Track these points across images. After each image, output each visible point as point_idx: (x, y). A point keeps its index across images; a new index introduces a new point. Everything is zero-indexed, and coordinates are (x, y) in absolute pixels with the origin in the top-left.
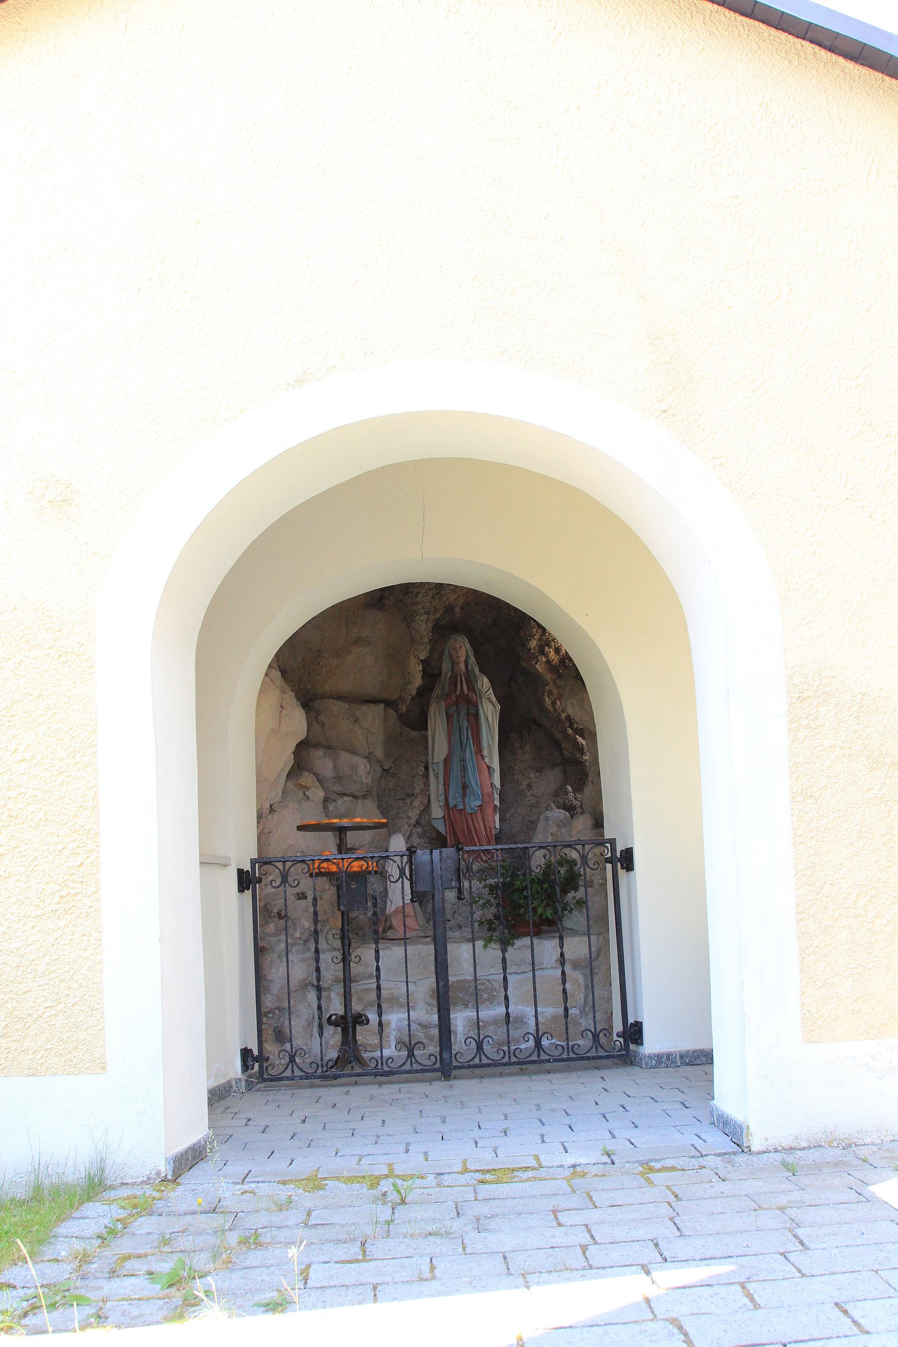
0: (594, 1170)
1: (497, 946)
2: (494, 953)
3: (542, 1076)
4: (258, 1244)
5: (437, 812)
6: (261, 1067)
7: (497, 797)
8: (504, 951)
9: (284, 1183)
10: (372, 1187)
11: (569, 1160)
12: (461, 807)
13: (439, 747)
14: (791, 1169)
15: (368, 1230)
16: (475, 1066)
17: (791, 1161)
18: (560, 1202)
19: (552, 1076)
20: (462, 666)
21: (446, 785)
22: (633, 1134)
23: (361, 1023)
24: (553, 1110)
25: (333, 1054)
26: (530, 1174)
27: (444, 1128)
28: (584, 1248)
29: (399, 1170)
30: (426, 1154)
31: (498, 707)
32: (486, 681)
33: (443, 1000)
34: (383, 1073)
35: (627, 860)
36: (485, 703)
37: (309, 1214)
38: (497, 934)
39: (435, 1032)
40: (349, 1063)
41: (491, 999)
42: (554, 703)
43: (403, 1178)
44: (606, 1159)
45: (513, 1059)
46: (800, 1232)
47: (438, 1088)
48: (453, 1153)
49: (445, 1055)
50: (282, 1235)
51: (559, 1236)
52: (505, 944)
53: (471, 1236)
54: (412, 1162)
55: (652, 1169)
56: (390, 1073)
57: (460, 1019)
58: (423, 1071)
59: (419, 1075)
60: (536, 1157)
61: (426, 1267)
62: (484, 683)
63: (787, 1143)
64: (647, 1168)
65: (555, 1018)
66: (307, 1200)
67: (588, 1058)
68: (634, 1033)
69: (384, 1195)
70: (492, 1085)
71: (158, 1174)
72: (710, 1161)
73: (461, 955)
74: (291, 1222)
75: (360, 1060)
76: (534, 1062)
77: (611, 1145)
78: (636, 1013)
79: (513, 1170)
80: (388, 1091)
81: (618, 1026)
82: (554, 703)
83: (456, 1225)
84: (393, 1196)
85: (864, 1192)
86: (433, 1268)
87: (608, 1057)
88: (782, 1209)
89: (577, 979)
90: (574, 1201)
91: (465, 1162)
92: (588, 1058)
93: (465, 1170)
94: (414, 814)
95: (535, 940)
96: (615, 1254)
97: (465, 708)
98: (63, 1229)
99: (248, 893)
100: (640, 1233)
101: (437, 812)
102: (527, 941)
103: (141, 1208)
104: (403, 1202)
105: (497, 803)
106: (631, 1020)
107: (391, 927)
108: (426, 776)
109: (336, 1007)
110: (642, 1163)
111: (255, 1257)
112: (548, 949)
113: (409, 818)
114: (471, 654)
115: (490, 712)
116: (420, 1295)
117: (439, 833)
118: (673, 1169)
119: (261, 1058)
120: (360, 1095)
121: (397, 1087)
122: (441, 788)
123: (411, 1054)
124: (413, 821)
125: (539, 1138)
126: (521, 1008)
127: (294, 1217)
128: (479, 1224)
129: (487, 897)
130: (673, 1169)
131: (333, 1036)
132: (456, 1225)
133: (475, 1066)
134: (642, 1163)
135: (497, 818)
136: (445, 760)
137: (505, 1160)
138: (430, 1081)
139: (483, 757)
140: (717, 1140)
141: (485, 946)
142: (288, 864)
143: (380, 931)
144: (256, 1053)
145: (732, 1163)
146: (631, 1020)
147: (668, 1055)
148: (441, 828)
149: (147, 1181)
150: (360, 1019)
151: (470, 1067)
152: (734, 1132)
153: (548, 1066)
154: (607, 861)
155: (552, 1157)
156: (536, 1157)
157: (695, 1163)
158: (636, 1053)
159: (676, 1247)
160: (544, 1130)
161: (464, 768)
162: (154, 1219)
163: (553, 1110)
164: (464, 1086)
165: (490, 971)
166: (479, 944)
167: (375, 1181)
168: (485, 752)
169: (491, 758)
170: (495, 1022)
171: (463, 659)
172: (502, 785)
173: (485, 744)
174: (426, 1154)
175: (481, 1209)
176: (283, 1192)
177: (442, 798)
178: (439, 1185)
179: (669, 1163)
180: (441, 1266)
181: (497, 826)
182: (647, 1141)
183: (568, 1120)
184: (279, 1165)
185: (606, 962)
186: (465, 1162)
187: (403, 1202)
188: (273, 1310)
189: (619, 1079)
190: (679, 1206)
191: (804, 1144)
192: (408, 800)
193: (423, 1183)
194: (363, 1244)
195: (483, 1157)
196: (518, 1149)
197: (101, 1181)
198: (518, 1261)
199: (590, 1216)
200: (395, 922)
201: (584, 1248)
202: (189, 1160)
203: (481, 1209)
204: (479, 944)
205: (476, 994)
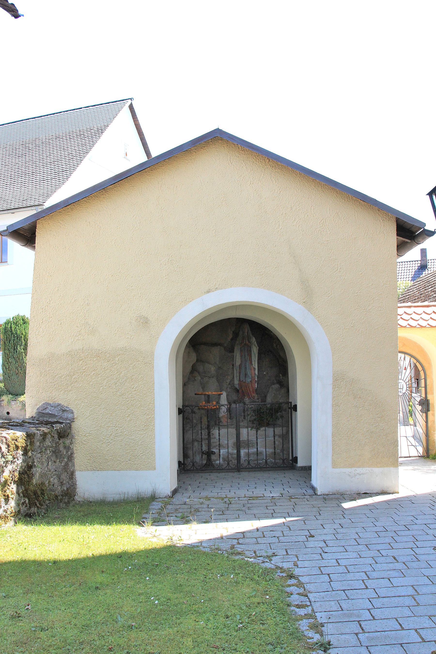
0: (277, 498)
1: (255, 430)
2: (254, 432)
3: (267, 472)
4: (199, 511)
5: (236, 382)
6: (184, 466)
7: (256, 377)
8: (257, 432)
9: (200, 498)
10: (222, 500)
11: (271, 495)
12: (244, 381)
13: (238, 362)
14: (325, 499)
15: (224, 509)
16: (247, 468)
17: (326, 497)
18: (268, 505)
19: (270, 472)
20: (246, 334)
21: (240, 373)
22: (289, 490)
23: (213, 454)
24: (269, 482)
25: (205, 462)
26: (261, 498)
27: (239, 486)
28: (272, 514)
29: (228, 496)
30: (235, 493)
31: (258, 348)
32: (254, 338)
33: (238, 445)
34: (220, 469)
35: (295, 408)
36: (253, 346)
37: (208, 505)
38: (255, 425)
39: (235, 456)
40: (209, 467)
41: (253, 446)
42: (277, 346)
43: (230, 498)
44: (281, 495)
45: (259, 467)
46: (320, 512)
47: (236, 474)
48: (242, 493)
49: (238, 465)
50: (203, 510)
51: (267, 511)
52: (257, 429)
53: (247, 511)
54: (232, 494)
55: (292, 498)
56: (223, 469)
57: (243, 452)
58: (232, 469)
59: (231, 471)
60: (263, 494)
61: (237, 516)
62: (254, 340)
63: (326, 493)
64: (291, 497)
65: (272, 453)
66: (207, 502)
67: (281, 467)
68: (295, 460)
69: (226, 502)
70: (252, 474)
71: (168, 495)
72: (306, 497)
73: (244, 432)
74: (205, 507)
75: (213, 465)
76: (265, 468)
77: (283, 492)
78: (296, 454)
79: (257, 497)
80: (222, 475)
81: (291, 458)
82: (277, 346)
83: (243, 508)
84: (228, 502)
85: (339, 505)
86: (239, 516)
87: (287, 467)
88: (318, 508)
89: (279, 441)
90: (271, 504)
91: (245, 495)
92: (281, 467)
93: (245, 497)
94: (228, 381)
95: (266, 428)
96: (279, 515)
97: (248, 349)
98: (151, 507)
99: (181, 415)
100: (285, 511)
101: (236, 382)
102: (264, 428)
103: (166, 504)
104: (230, 503)
105: (256, 379)
106: (294, 456)
107: (221, 421)
108: (233, 368)
109: (205, 448)
110: (289, 497)
111: (198, 514)
112: (270, 431)
113: (227, 382)
114: (249, 329)
115: (255, 350)
116: (236, 521)
117: (236, 388)
118: (297, 498)
119: (184, 464)
120: (214, 476)
121: (224, 474)
122: (238, 375)
123: (228, 464)
124: (228, 384)
125: (264, 490)
126: (261, 449)
127: (205, 506)
128: (249, 508)
129: (252, 414)
130: (297, 498)
131: (205, 457)
132: (243, 508)
133: (247, 468)
134: (289, 497)
135: (256, 384)
136: (239, 366)
137: (255, 495)
138: (234, 472)
139: (252, 364)
140: (310, 492)
141: (251, 430)
142: (193, 407)
143: (218, 423)
144: (182, 462)
145: (312, 497)
146: (294, 456)
147: (305, 467)
148: (237, 386)
149: (166, 497)
150: (213, 453)
151: (246, 468)
152: (313, 489)
153: (268, 469)
154: (289, 408)
155: (268, 494)
156: (263, 494)
157: (303, 497)
158: (295, 466)
159: (294, 514)
160: (266, 487)
161: (246, 368)
162: (171, 506)
163: (269, 482)
164: (244, 474)
165: (253, 438)
166: (249, 429)
167: (223, 499)
168: (253, 363)
169: (255, 365)
170: (253, 453)
171: (246, 331)
172: (258, 373)
173: (253, 360)
174: (235, 493)
175: (250, 505)
176: (201, 500)
177: (238, 378)
178: (239, 500)
179: (296, 497)
180: (241, 516)
181: (256, 387)
182: (292, 491)
183: (273, 485)
184: (197, 494)
185: (288, 436)
186: (245, 495)
187: (230, 503)
188: (206, 523)
189: (289, 474)
190: (295, 506)
191: (331, 493)
192: (227, 376)
193: (235, 499)
194: (223, 512)
195: (250, 494)
196: (259, 492)
197: (155, 496)
198: (257, 515)
199: (274, 508)
200: (222, 420)
201: (272, 514)
202: (175, 492)
203: (250, 505)
204: (249, 429)
205: (248, 444)
